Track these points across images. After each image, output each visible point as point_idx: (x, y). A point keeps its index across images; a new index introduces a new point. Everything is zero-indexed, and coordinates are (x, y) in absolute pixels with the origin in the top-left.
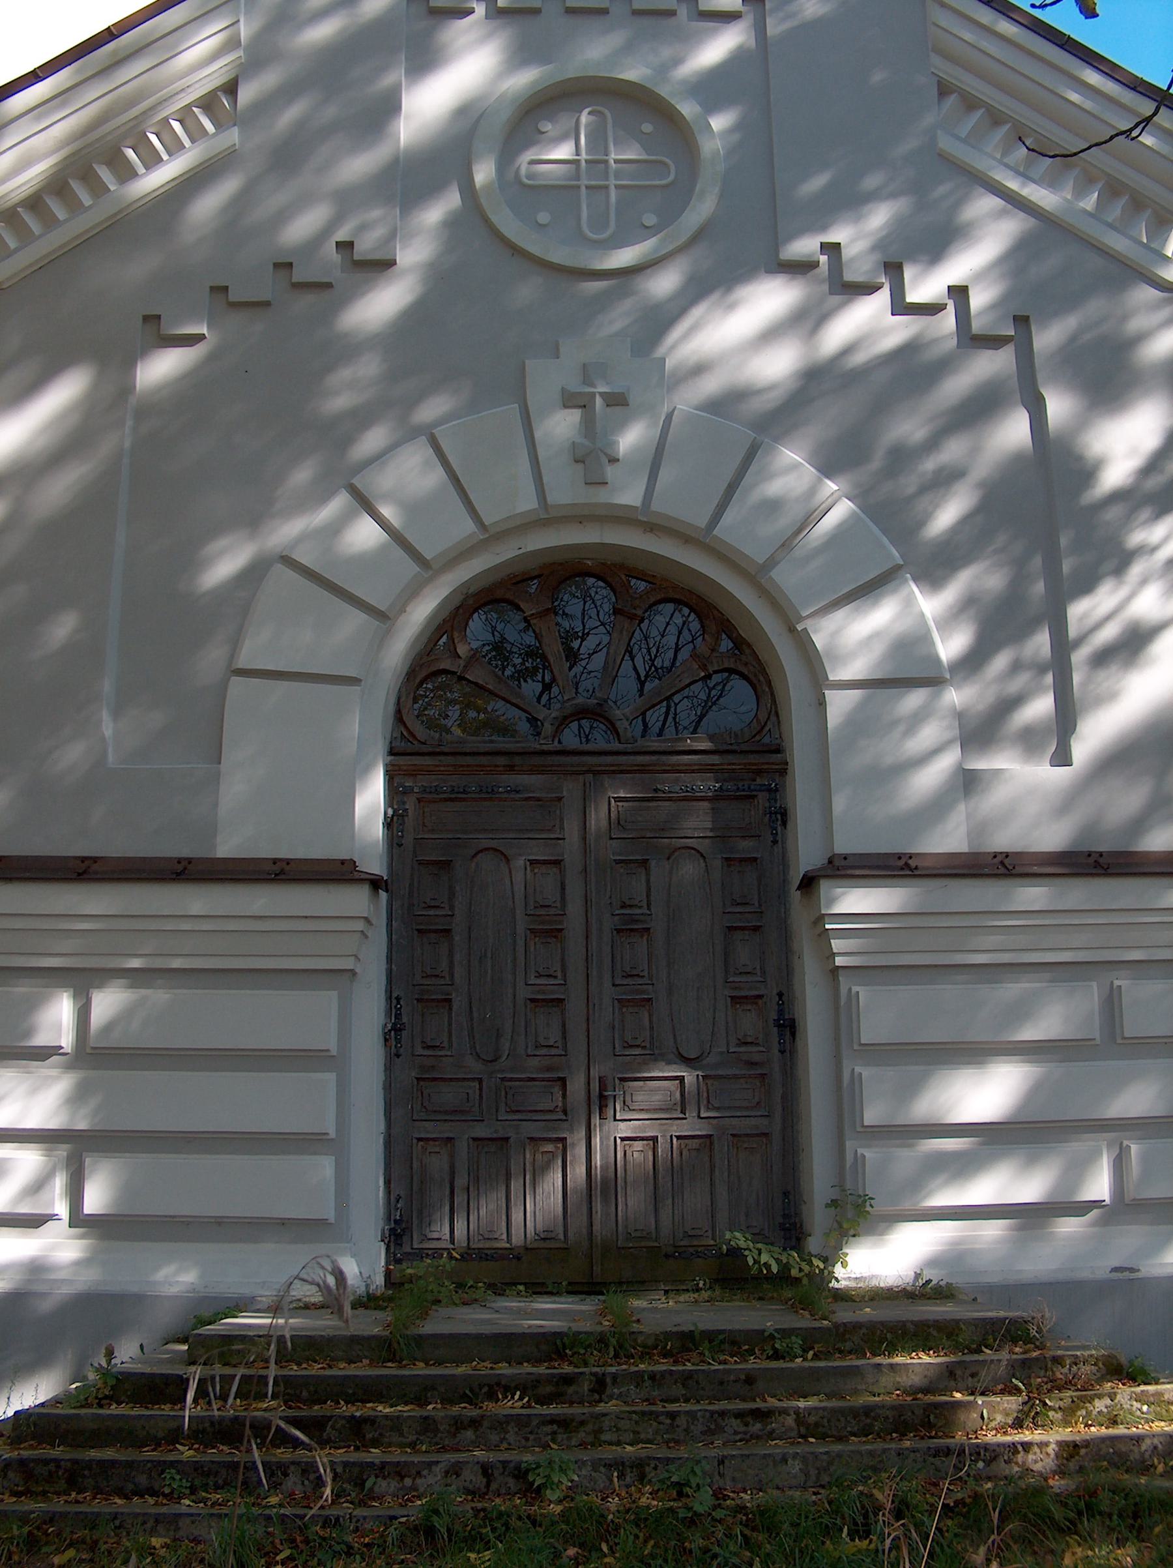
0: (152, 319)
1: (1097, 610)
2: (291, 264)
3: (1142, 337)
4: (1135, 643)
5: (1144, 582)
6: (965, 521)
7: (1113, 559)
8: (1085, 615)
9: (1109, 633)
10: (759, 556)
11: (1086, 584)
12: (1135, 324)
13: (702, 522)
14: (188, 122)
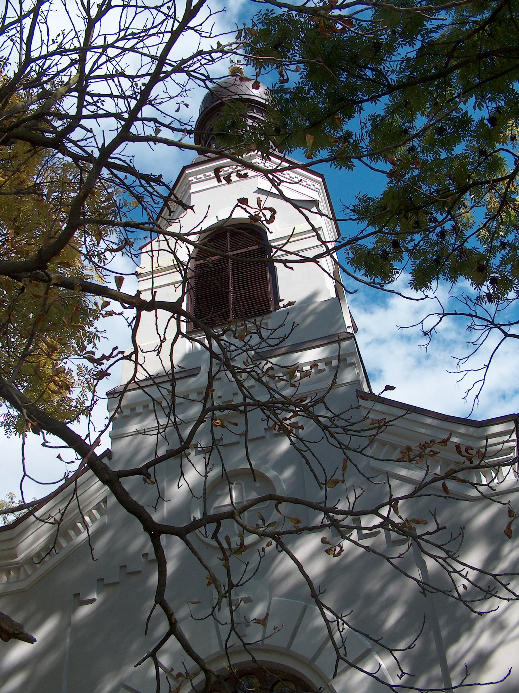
0: (77, 595)
1: (462, 649)
2: (126, 566)
3: (470, 520)
4: (482, 660)
5: (482, 631)
6: (399, 621)
7: (464, 625)
8: (456, 653)
9: (469, 659)
10: (309, 655)
11: (455, 638)
12: (466, 515)
13: (285, 645)
14: (92, 516)
